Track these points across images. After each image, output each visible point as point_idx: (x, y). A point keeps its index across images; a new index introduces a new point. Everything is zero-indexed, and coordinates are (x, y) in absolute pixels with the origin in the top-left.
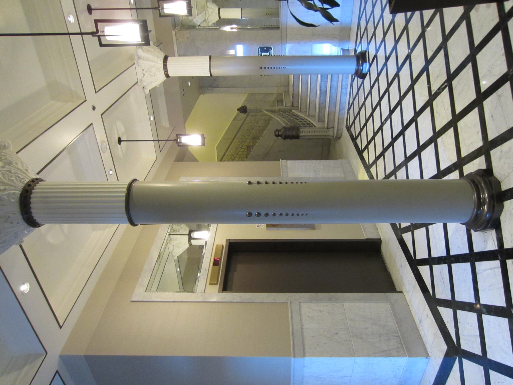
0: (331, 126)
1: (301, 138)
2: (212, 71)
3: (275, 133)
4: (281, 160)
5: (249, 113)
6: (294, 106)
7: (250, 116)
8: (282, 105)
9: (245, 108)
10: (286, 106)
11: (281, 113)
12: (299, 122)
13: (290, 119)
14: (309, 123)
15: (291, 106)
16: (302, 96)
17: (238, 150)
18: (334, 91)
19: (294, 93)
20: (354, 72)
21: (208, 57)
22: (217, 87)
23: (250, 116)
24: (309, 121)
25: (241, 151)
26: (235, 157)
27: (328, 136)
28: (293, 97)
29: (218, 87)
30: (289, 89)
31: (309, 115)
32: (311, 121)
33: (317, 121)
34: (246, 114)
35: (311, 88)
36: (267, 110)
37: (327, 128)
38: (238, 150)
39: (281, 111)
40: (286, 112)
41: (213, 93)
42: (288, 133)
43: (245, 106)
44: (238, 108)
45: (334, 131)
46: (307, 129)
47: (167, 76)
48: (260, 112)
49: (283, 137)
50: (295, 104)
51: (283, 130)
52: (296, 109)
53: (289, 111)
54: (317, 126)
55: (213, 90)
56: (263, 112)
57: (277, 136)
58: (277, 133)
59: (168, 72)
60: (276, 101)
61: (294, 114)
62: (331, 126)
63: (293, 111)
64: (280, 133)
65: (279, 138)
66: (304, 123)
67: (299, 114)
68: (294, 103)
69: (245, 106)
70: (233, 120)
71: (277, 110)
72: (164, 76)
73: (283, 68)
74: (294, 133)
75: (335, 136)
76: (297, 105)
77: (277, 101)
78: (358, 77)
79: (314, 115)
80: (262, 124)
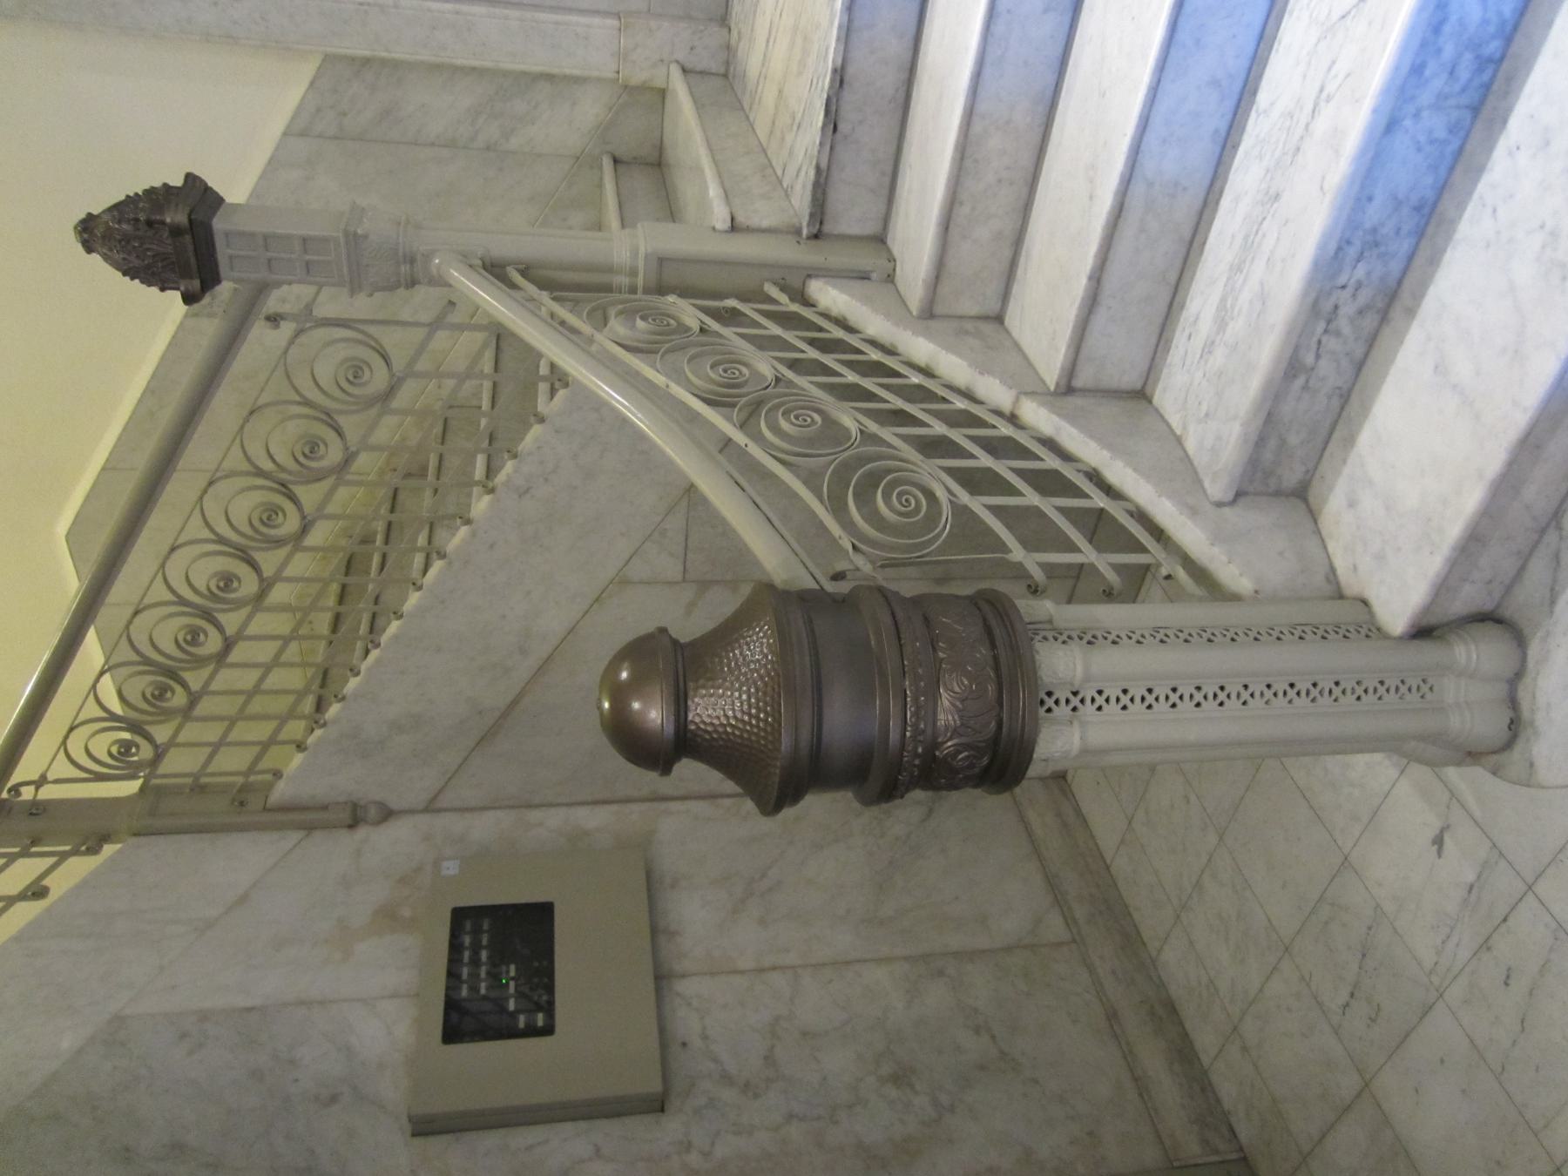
5: (261, 290)
6: (827, 228)
8: (670, 210)
9: (176, 216)
10: (734, 227)
11: (689, 314)
13: (833, 433)
14: (920, 387)
17: (293, 498)
19: (851, 70)
23: (274, 320)
25: (289, 572)
26: (230, 630)
31: (929, 313)
32: (1119, 473)
36: (495, 270)
38: (293, 498)
39: (685, 292)
40: (745, 308)
43: (190, 178)
50: (851, 215)
51: (757, 648)
52: (864, 277)
53: (774, 292)
54: (1232, 575)
56: (441, 282)
58: (653, 713)
60: (607, 163)
61: (890, 362)
63: (830, 296)
65: (689, 770)
66: (1038, 513)
67: (920, 348)
68: (839, 196)
69: (190, 178)
71: (633, 272)
77: (616, 161)
80: (469, 386)
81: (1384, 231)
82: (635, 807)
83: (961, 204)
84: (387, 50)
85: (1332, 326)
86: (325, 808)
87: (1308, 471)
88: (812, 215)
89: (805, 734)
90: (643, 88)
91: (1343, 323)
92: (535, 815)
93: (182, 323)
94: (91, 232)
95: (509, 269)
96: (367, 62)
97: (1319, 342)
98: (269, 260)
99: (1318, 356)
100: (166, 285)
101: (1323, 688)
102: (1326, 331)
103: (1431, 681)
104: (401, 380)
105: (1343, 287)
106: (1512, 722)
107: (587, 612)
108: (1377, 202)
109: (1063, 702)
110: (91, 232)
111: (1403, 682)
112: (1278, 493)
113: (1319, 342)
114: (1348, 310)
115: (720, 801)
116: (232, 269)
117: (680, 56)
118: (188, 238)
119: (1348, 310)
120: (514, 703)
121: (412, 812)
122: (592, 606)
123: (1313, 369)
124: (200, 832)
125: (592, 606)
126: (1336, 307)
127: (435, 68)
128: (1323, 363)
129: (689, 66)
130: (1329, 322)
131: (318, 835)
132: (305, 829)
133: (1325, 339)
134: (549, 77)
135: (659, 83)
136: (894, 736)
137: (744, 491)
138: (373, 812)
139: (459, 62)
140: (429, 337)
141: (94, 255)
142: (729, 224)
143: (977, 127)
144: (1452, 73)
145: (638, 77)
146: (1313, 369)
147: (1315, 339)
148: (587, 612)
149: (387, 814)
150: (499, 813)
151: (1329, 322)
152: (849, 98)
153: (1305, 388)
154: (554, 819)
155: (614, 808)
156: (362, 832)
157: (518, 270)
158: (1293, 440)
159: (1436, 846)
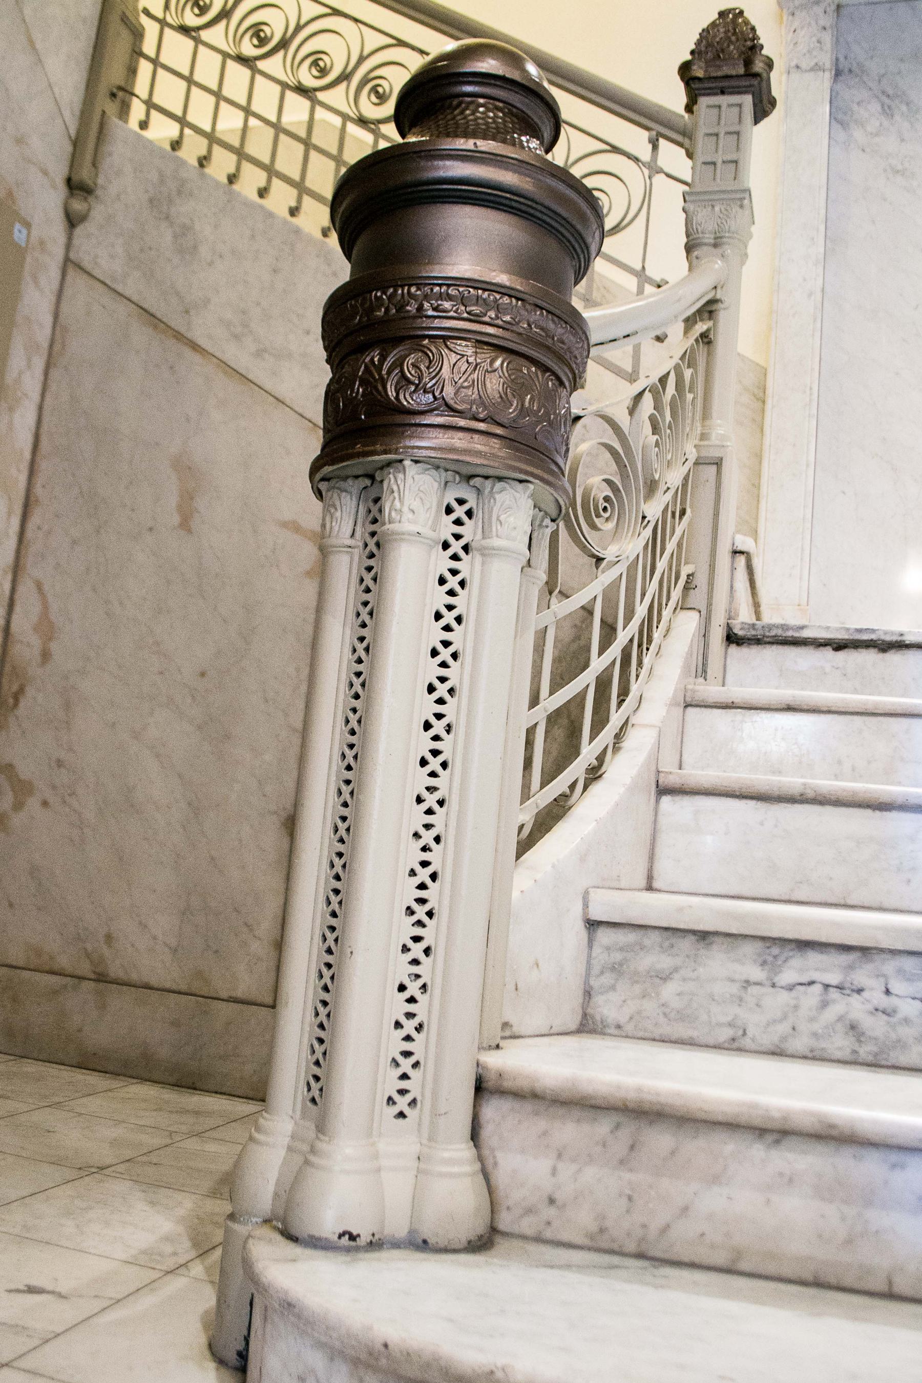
6: (733, 649)
82: (23, 478)
84: (773, 407)
85: (834, 994)
86: (94, 164)
87: (619, 1027)
91: (840, 1005)
92: (39, 364)
95: (710, 324)
97: (811, 983)
98: (717, 135)
99: (791, 988)
100: (696, 55)
101: (424, 926)
102: (827, 986)
105: (888, 992)
107: (303, 417)
109: (458, 529)
111: (416, 1065)
112: (588, 994)
113: (811, 983)
114: (856, 1007)
115: (9, 577)
116: (709, 107)
118: (742, 71)
119: (856, 1007)
120: (195, 347)
121: (68, 246)
122: (310, 421)
123: (774, 985)
124: (95, 47)
125: (310, 421)
126: (860, 991)
128: (784, 997)
130: (840, 988)
131: (70, 149)
132: (77, 138)
133: (817, 988)
137: (624, 337)
138: (78, 206)
139: (765, 464)
141: (717, 16)
146: (774, 985)
147: (816, 976)
148: (303, 417)
149: (72, 221)
150: (48, 331)
151: (840, 988)
154: (31, 384)
155: (27, 455)
156: (62, 190)
157: (708, 330)
158: (669, 991)
159: (26, 1288)
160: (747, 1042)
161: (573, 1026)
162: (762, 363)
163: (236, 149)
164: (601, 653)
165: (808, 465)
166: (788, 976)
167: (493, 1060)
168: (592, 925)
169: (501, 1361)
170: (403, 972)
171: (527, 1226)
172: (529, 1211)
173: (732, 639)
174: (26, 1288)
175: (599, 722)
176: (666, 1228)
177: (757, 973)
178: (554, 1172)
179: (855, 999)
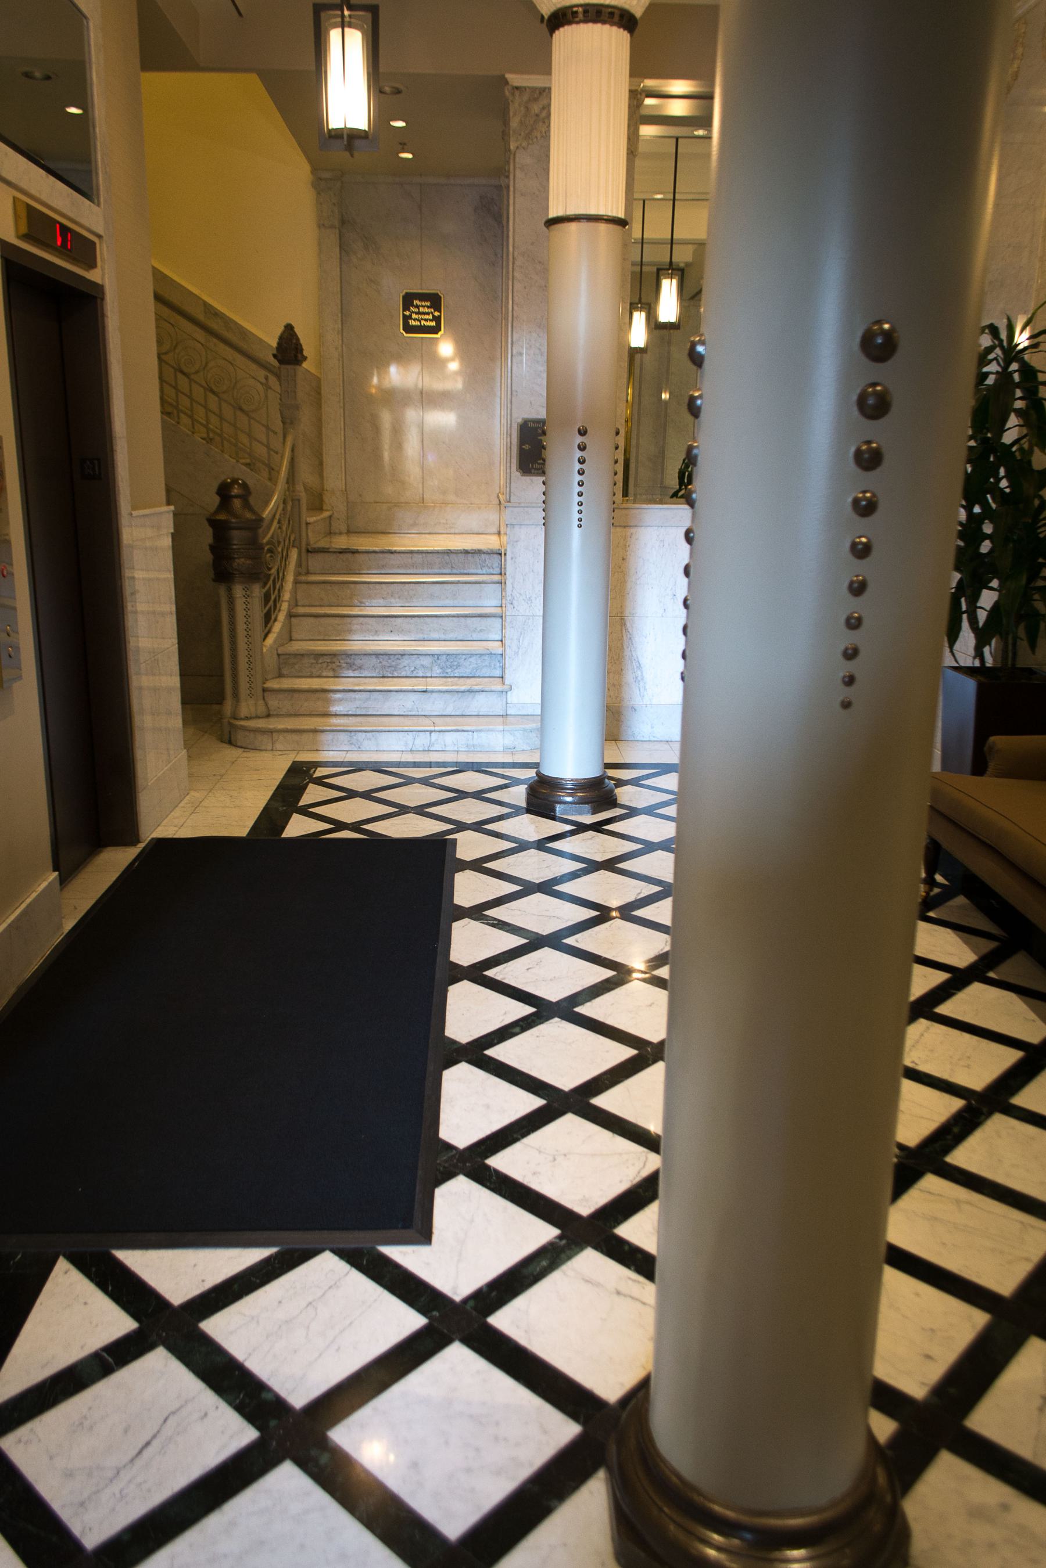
0: (273, 702)
1: (222, 591)
2: (573, 226)
3: (235, 481)
4: (172, 508)
5: (278, 377)
6: (310, 554)
7: (266, 378)
12: (272, 578)
14: (270, 618)
15: (308, 544)
16: (358, 586)
18: (409, 705)
20: (551, 771)
21: (621, 215)
22: (344, 248)
23: (266, 378)
24: (276, 620)
27: (236, 695)
28: (342, 552)
29: (340, 250)
30: (341, 533)
33: (281, 650)
34: (275, 362)
35: (399, 620)
37: (264, 690)
41: (321, 226)
42: (237, 537)
44: (296, 330)
45: (258, 717)
46: (258, 611)
47: (561, 18)
48: (284, 423)
49: (222, 517)
51: (249, 515)
55: (332, 227)
57: (224, 491)
58: (236, 491)
59: (582, 26)
62: (273, 702)
64: (237, 503)
65: (217, 499)
68: (320, 557)
70: (205, 304)
72: (559, 6)
73: (580, 516)
74: (241, 562)
75: (242, 723)
76: (311, 569)
78: (681, 797)
79: (293, 638)
81: (354, 667)
83: (331, 586)
85: (329, 664)
88: (314, 548)
89: (233, 525)
90: (321, 501)
93: (201, 299)
94: (289, 328)
96: (319, 393)
97: (325, 662)
99: (321, 663)
102: (328, 663)
103: (253, 697)
104: (248, 415)
106: (247, 717)
108: (361, 661)
110: (289, 328)
117: (336, 514)
127: (320, 420)
128: (320, 665)
129: (332, 518)
130: (330, 662)
134: (321, 464)
135: (325, 507)
136: (235, 547)
140: (263, 425)
142: (308, 522)
143: (352, 586)
144: (390, 667)
145: (326, 499)
151: (330, 662)
152: (349, 556)
153: (312, 663)
158: (297, 667)
159: (358, 662)
160: (313, 675)
161: (277, 676)
162: (318, 375)
163: (560, 1237)
164: (270, 586)
165: (341, 430)
166: (320, 661)
167: (265, 686)
168: (279, 655)
169: (286, 323)
170: (248, 673)
171: (275, 713)
172: (275, 710)
173: (308, 551)
174: (358, 662)
175: (275, 609)
176: (299, 710)
177: (314, 661)
178: (279, 703)
179: (334, 665)
